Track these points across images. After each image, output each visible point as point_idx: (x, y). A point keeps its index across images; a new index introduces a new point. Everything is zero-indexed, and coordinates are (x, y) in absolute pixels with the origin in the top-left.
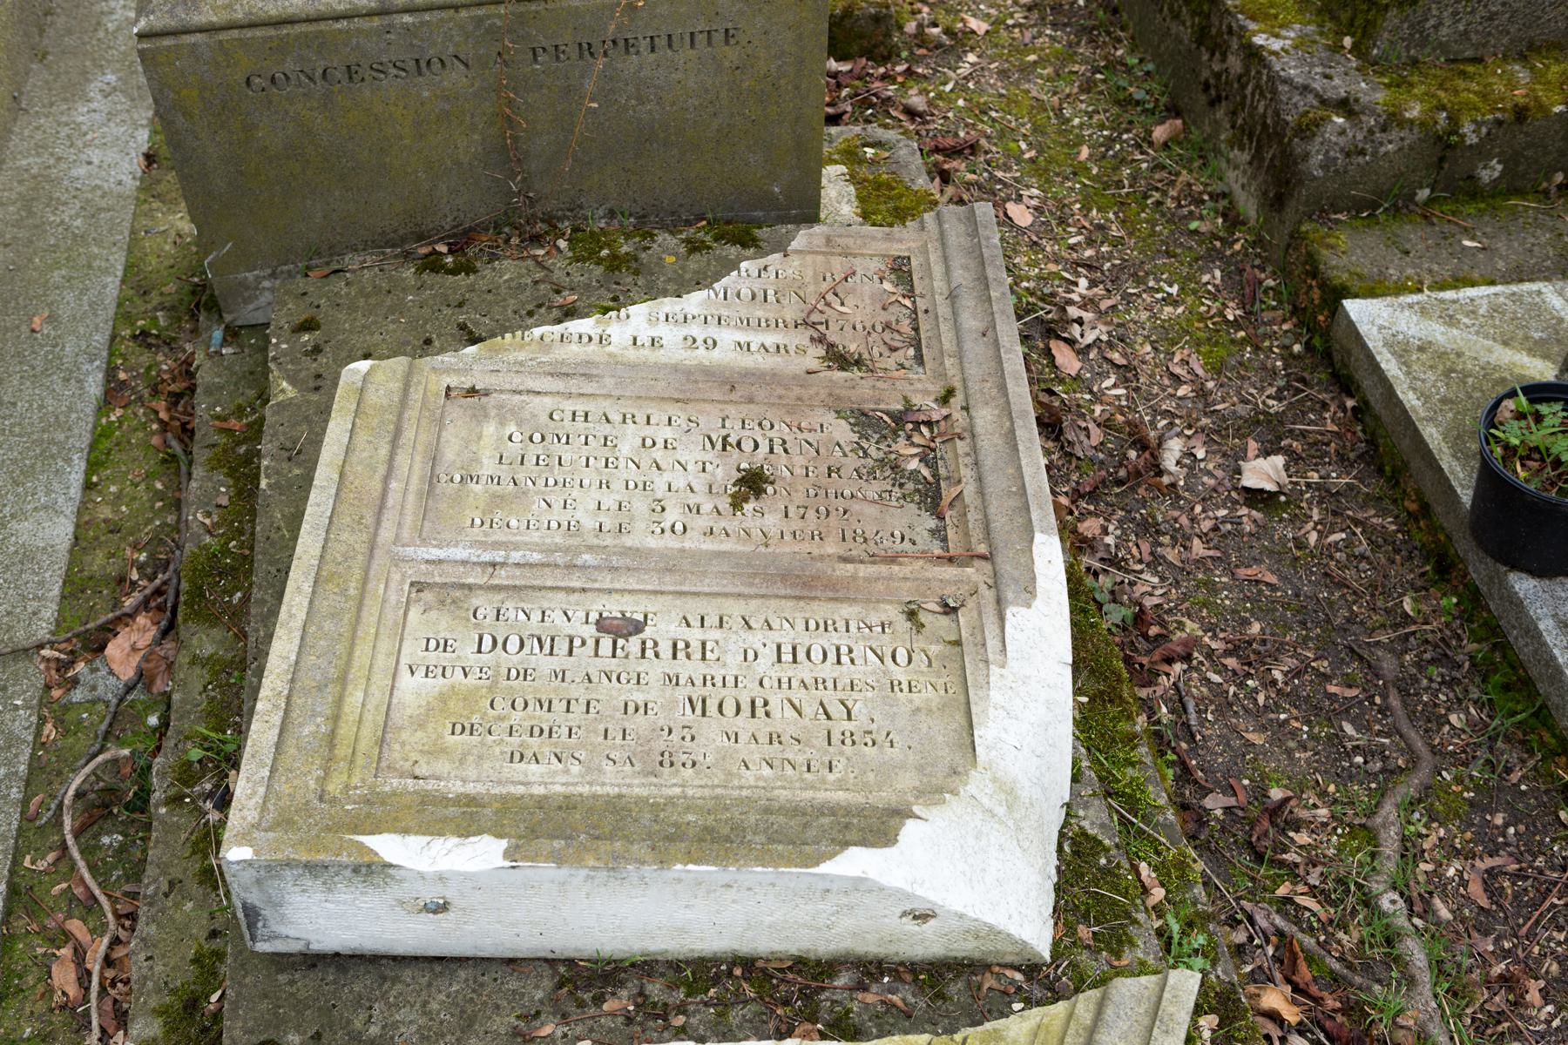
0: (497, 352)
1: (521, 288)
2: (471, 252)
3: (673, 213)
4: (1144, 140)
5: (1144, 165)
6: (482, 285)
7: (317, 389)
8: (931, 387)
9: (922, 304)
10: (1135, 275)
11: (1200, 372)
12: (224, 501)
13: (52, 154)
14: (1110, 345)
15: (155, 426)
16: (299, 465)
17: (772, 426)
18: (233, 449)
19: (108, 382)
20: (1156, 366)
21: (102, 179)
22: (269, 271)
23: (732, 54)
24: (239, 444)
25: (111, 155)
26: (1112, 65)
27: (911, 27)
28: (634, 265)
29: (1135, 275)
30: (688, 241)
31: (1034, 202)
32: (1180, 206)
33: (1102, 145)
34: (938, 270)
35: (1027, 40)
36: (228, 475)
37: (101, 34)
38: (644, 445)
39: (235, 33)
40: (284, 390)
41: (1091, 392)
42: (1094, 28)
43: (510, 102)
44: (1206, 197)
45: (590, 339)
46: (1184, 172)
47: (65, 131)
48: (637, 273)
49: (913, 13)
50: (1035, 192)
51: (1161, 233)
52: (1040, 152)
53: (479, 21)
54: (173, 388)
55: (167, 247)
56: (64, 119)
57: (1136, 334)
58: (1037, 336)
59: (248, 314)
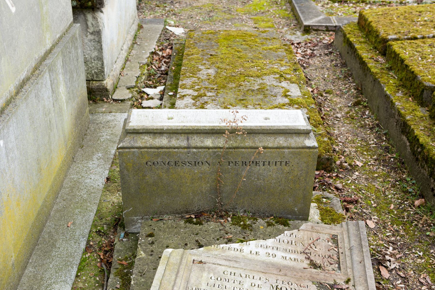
0: (209, 250)
1: (216, 231)
2: (201, 218)
3: (264, 213)
4: (412, 204)
5: (412, 212)
6: (204, 229)
7: (151, 255)
8: (343, 278)
9: (341, 251)
10: (408, 247)
11: (430, 282)
12: (118, 286)
13: (81, 175)
14: (399, 270)
15: (99, 260)
16: (144, 278)
17: (292, 284)
18: (123, 270)
19: (87, 244)
20: (415, 278)
21: (94, 184)
22: (141, 217)
23: (287, 169)
24: (125, 269)
25: (97, 177)
26: (401, 180)
27: (338, 162)
28: (251, 228)
29: (408, 247)
30: (267, 222)
31: (376, 221)
32: (423, 227)
33: (398, 205)
34: (346, 240)
35: (374, 170)
36: (120, 278)
37: (99, 142)
38: (252, 285)
39: (146, 150)
40: (141, 254)
41: (393, 285)
42: (396, 168)
43: (220, 176)
44: (432, 225)
45: (237, 250)
46: (425, 216)
47: (85, 169)
48: (251, 230)
49: (339, 158)
50: (376, 217)
51: (417, 235)
52: (378, 205)
53: (215, 152)
54: (106, 249)
55: (109, 206)
56: (85, 165)
57: (408, 267)
58: (375, 264)
59: (133, 229)
